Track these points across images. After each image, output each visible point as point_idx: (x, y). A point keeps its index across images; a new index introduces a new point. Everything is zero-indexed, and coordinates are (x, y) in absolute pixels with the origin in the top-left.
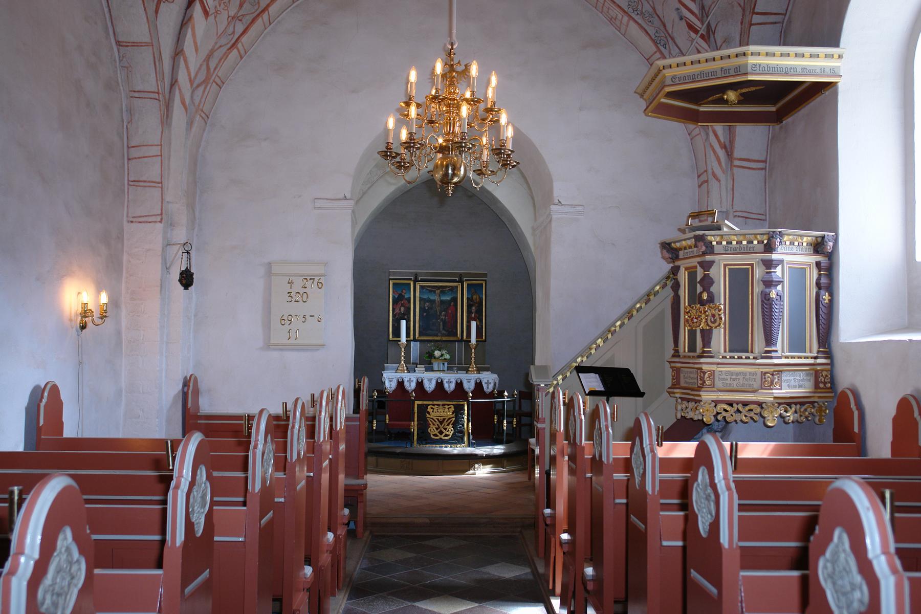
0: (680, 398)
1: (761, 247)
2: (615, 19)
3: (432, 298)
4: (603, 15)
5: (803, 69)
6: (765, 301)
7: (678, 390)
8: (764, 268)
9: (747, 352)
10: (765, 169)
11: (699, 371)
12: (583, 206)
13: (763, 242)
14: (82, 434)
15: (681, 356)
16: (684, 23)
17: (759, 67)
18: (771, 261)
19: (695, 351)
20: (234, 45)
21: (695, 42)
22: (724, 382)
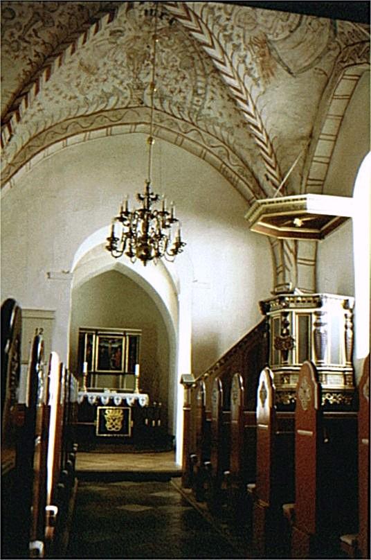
3: (106, 345)
14: (26, 318)
16: (270, 183)
18: (183, 506)
20: (8, 180)
21: (280, 187)
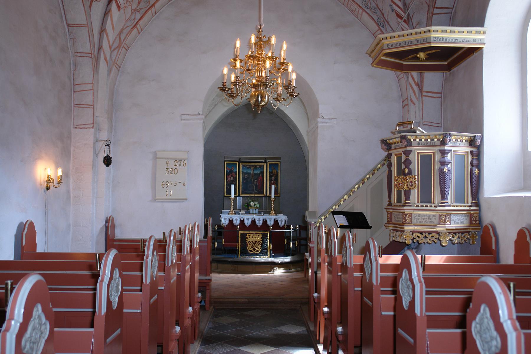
0: (392, 229)
1: (439, 143)
2: (355, 11)
3: (249, 172)
4: (348, 9)
5: (463, 40)
6: (441, 174)
7: (391, 225)
8: (441, 154)
9: (431, 203)
10: (441, 97)
11: (403, 214)
12: (336, 119)
13: (440, 140)
15: (393, 206)
16: (394, 13)
17: (438, 39)
18: (445, 150)
19: (401, 202)
20: (135, 26)
21: (401, 24)
22: (417, 220)
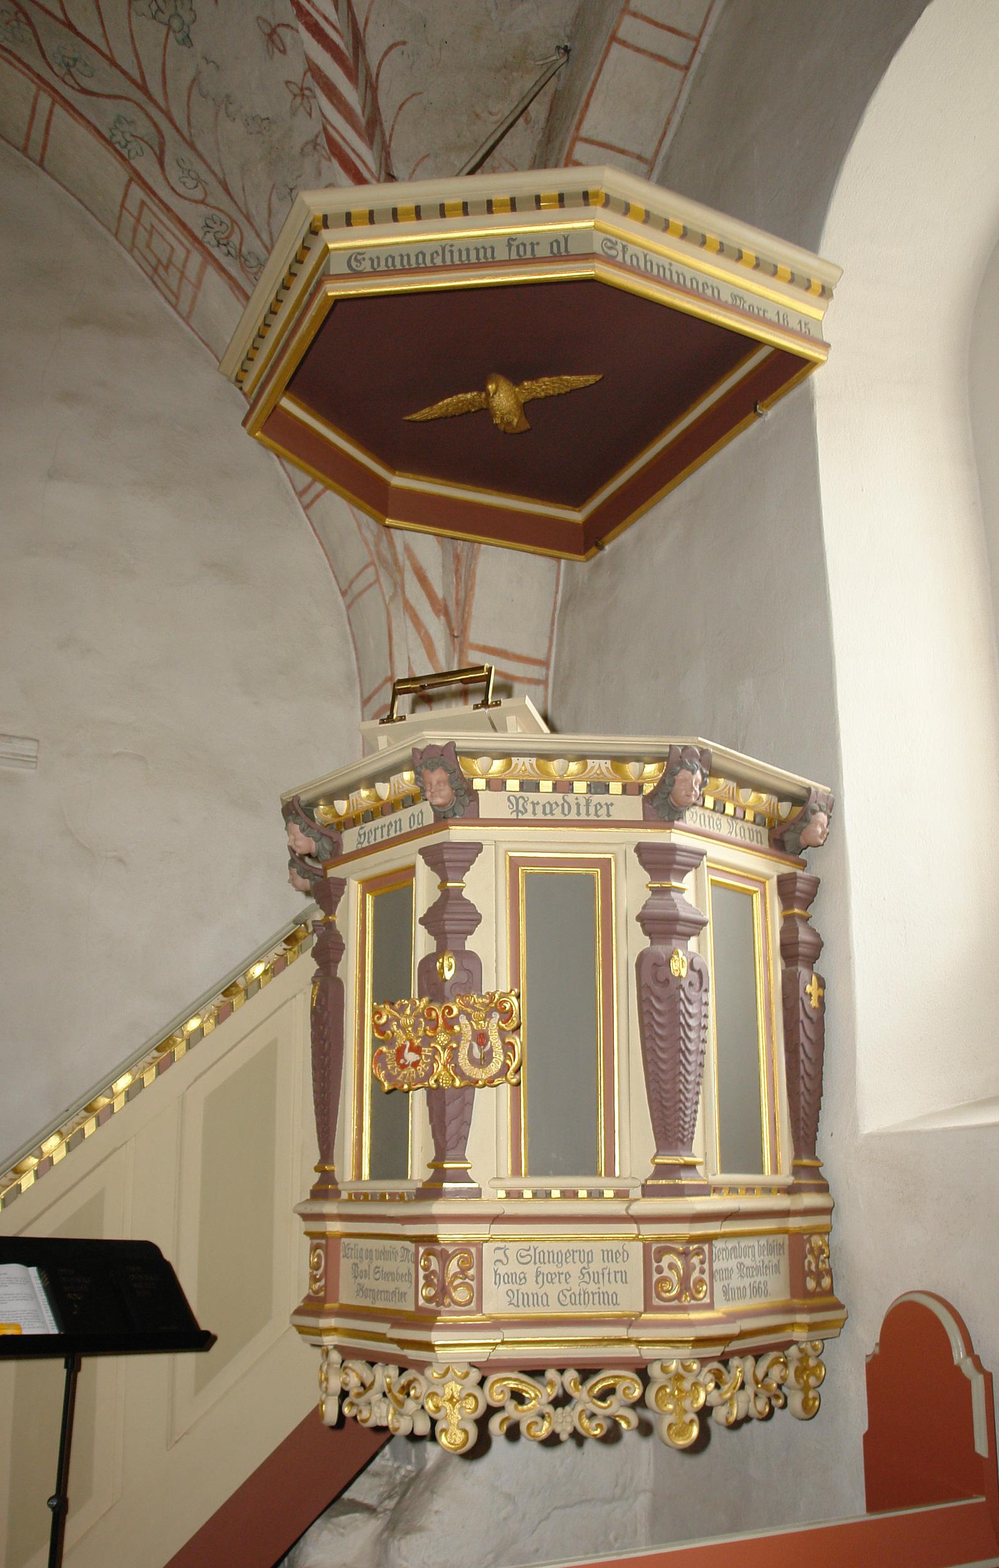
0: (336, 1347)
1: (633, 808)
2: (166, 268)
4: (133, 257)
5: (735, 297)
6: (657, 989)
7: (332, 1322)
8: (646, 876)
9: (594, 1172)
10: (545, 682)
11: (421, 1250)
12: (38, 741)
13: (640, 788)
15: (344, 1195)
17: (624, 253)
19: (401, 1172)
22: (515, 1287)
